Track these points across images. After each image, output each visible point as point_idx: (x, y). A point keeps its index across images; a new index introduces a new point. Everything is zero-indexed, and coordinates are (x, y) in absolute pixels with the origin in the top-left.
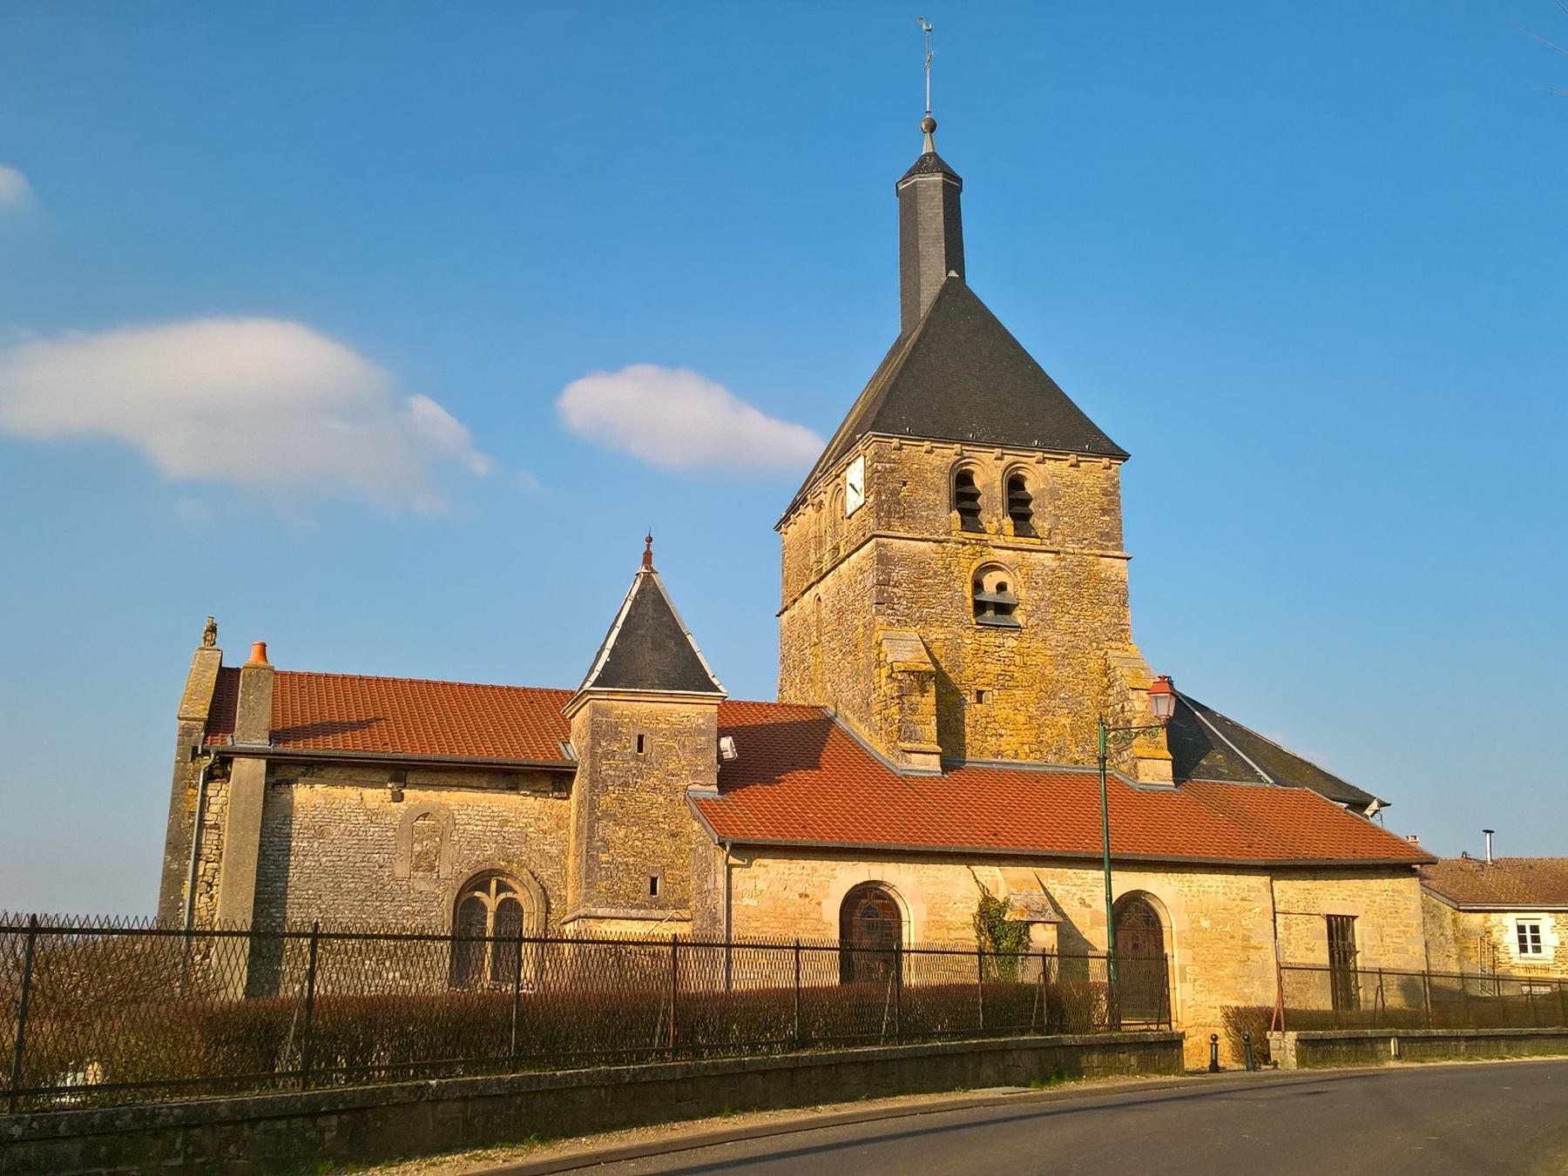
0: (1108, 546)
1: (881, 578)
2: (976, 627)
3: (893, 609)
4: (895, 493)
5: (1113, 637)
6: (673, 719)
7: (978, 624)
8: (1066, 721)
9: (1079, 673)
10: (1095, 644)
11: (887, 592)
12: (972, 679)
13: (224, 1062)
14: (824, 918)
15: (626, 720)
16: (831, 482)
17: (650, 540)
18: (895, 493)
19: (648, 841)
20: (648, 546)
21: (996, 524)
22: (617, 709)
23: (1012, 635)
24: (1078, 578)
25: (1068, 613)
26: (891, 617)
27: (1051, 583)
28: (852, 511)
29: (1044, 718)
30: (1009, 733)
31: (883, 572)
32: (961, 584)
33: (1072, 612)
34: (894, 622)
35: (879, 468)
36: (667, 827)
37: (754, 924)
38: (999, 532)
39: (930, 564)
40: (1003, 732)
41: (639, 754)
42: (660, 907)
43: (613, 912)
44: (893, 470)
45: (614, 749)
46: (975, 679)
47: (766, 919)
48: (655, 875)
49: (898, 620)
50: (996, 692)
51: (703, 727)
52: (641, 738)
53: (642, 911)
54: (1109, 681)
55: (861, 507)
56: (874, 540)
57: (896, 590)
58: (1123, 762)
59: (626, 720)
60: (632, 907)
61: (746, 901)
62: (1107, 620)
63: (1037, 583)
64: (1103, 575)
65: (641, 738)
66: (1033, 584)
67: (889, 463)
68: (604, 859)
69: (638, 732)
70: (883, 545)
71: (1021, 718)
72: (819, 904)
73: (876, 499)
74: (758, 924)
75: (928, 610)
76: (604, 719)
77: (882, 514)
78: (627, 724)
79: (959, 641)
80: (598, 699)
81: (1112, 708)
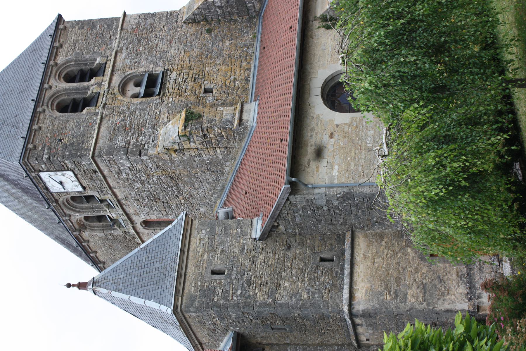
0: (116, 25)
1: (122, 153)
2: (161, 96)
3: (144, 145)
4: (65, 147)
5: (175, 20)
6: (201, 250)
7: (159, 94)
8: (227, 43)
9: (196, 37)
10: (179, 29)
11: (133, 149)
12: (196, 96)
13: (484, 185)
14: (347, 122)
15: (199, 283)
16: (62, 210)
17: (69, 285)
18: (65, 147)
19: (293, 265)
20: (74, 286)
21: (94, 87)
22: (190, 291)
23: (169, 74)
24: (134, 40)
25: (157, 45)
26: (150, 146)
27: (137, 55)
28: (79, 186)
29: (224, 55)
30: (233, 74)
31: (118, 151)
32: (132, 105)
33: (156, 42)
34: (153, 144)
35: (47, 156)
36: (282, 252)
37: (352, 167)
38: (100, 85)
39: (116, 124)
40: (232, 77)
41: (226, 273)
42: (342, 254)
43: (346, 288)
44: (50, 149)
45: (221, 291)
46: (196, 95)
47: (349, 159)
48: (318, 258)
49: (153, 141)
50: (206, 82)
51: (208, 230)
52: (213, 273)
53: (346, 266)
54: (202, 20)
55: (76, 175)
56: (96, 158)
57: (132, 143)
58: (255, 8)
59: (199, 283)
60: (343, 274)
61: (335, 173)
62: (163, 24)
63: (136, 62)
64: (134, 27)
65: (213, 273)
66: (136, 64)
67: (44, 151)
68: (306, 296)
69: (209, 275)
70: (100, 152)
71: (223, 68)
72: (338, 126)
73: (68, 159)
74: (352, 164)
75: (147, 124)
76: (198, 299)
77: (79, 153)
78: (202, 283)
79: (170, 105)
80: (182, 304)
81: (220, 18)
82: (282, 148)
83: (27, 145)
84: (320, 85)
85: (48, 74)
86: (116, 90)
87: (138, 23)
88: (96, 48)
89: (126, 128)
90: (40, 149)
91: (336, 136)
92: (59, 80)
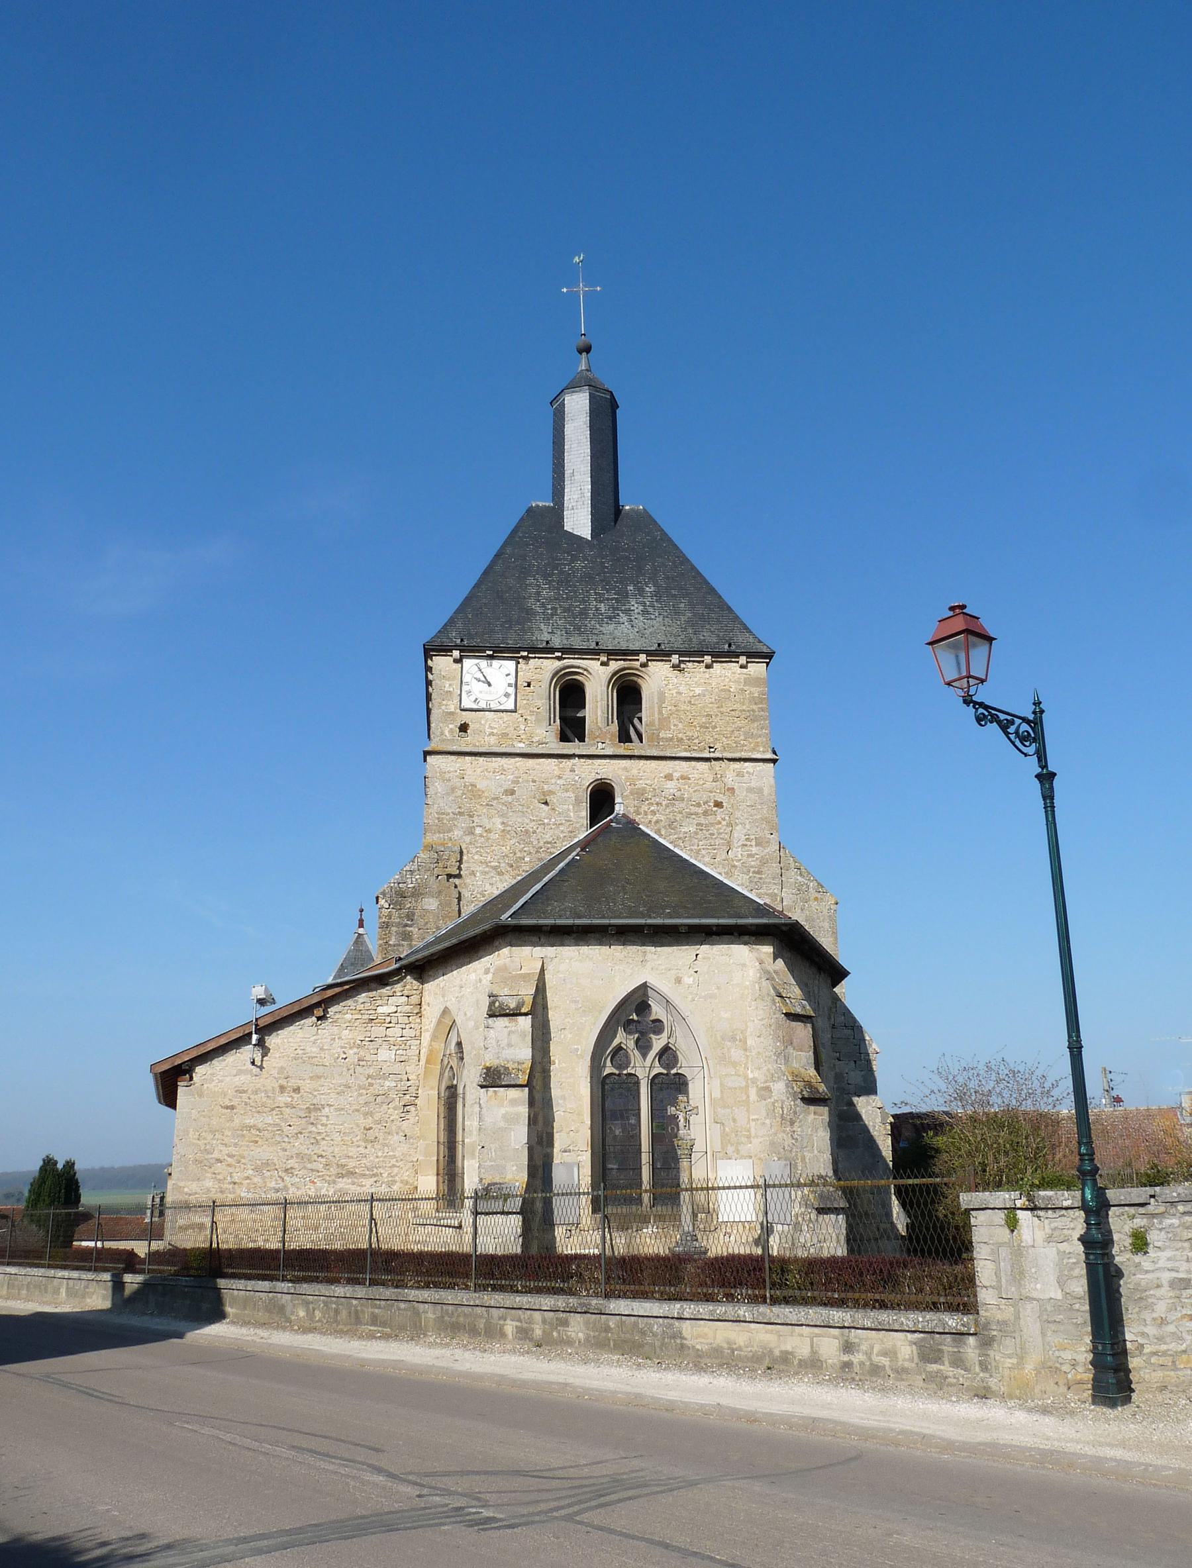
17: (362, 911)
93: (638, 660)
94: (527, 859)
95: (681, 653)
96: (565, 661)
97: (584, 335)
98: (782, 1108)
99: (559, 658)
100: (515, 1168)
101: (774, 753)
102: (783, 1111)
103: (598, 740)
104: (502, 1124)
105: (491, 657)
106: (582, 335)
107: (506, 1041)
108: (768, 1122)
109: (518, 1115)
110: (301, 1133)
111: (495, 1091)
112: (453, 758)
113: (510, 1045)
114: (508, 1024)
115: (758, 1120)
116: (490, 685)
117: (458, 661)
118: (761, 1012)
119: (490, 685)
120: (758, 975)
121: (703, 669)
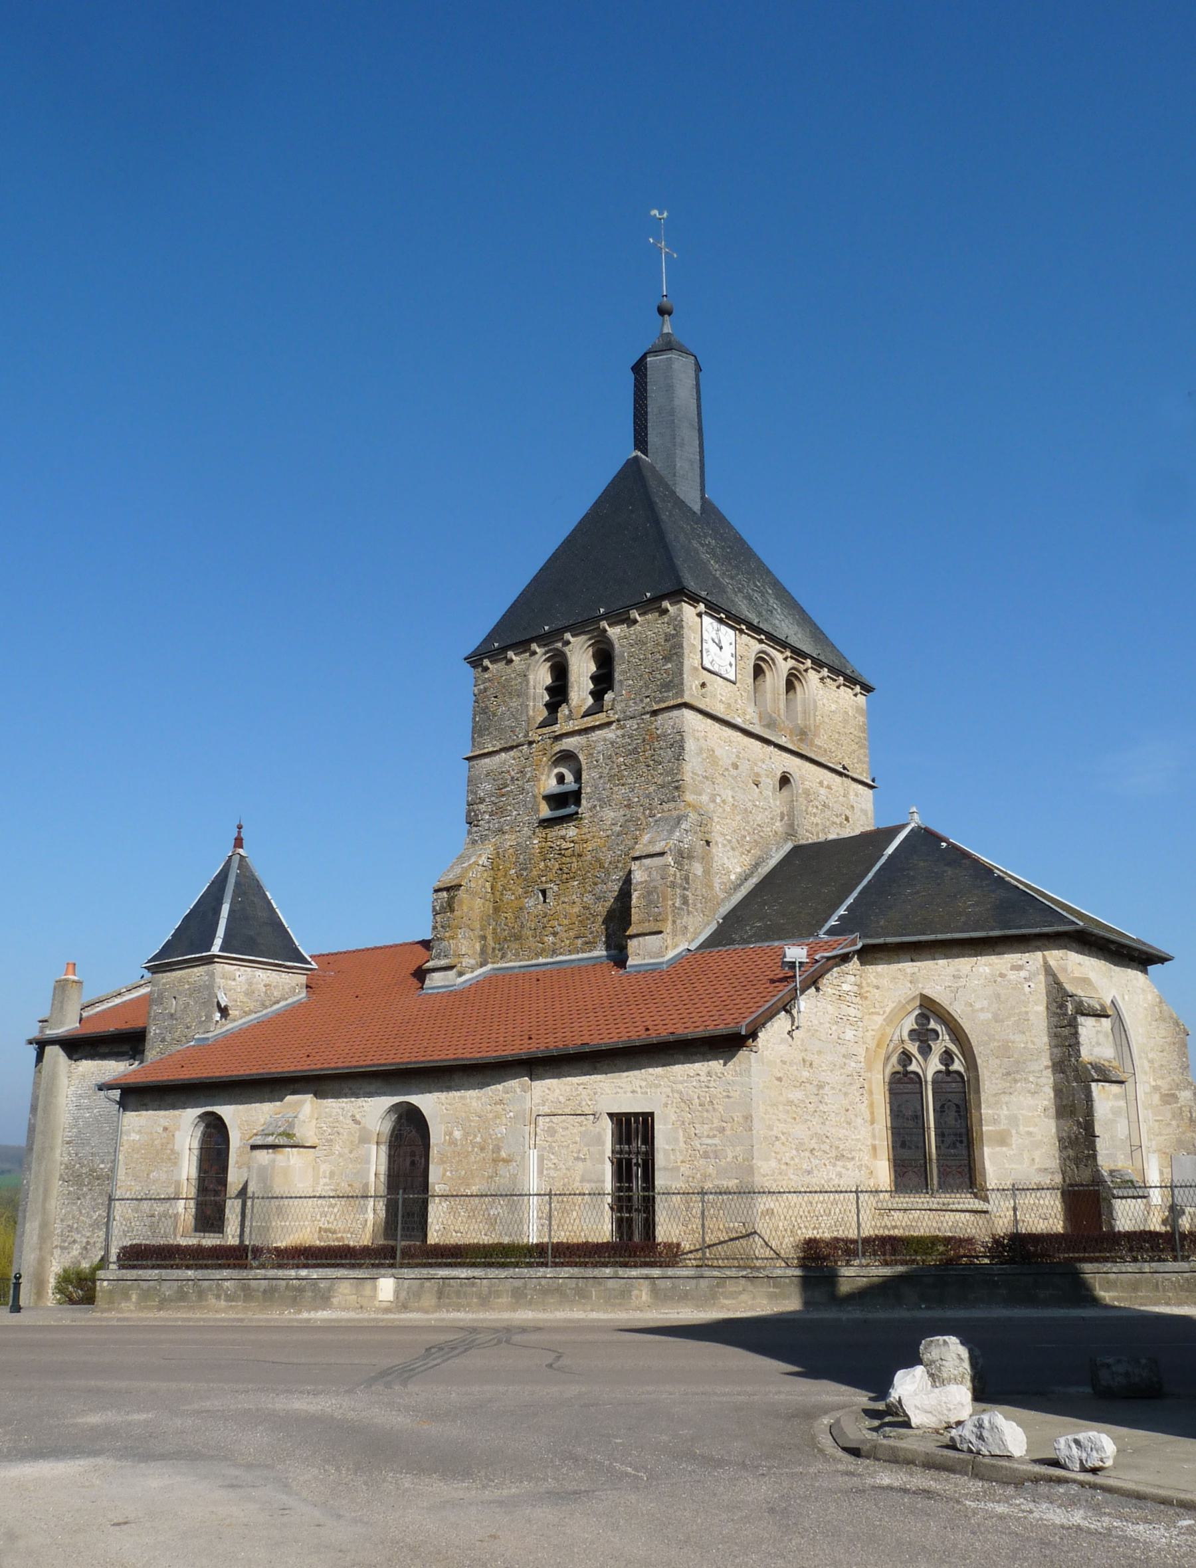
17: (240, 827)
20: (239, 833)
22: (163, 978)
72: (173, 1135)
82: (655, 992)
83: (485, 658)
84: (215, 1111)
85: (587, 627)
86: (557, 748)
87: (665, 736)
88: (631, 682)
89: (502, 789)
90: (486, 676)
91: (165, 1135)
92: (545, 661)
93: (803, 663)
94: (748, 839)
95: (831, 669)
96: (763, 645)
97: (666, 296)
98: (1190, 1112)
99: (761, 641)
100: (1123, 1157)
101: (873, 781)
102: (1191, 1115)
103: (783, 733)
104: (1110, 1116)
105: (720, 621)
106: (663, 296)
107: (1095, 1040)
108: (1174, 1123)
109: (989, 1107)
110: (816, 1111)
111: (1103, 1086)
112: (700, 717)
113: (1098, 1044)
114: (1094, 1024)
115: (1162, 1121)
116: (721, 648)
117: (700, 615)
118: (1163, 1031)
119: (721, 648)
120: (1158, 1000)
121: (835, 688)
